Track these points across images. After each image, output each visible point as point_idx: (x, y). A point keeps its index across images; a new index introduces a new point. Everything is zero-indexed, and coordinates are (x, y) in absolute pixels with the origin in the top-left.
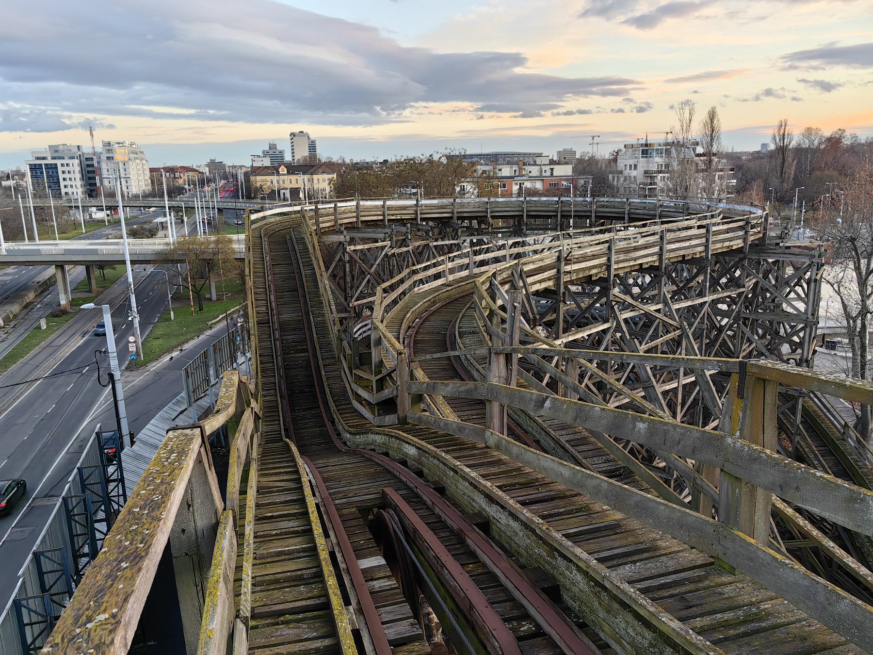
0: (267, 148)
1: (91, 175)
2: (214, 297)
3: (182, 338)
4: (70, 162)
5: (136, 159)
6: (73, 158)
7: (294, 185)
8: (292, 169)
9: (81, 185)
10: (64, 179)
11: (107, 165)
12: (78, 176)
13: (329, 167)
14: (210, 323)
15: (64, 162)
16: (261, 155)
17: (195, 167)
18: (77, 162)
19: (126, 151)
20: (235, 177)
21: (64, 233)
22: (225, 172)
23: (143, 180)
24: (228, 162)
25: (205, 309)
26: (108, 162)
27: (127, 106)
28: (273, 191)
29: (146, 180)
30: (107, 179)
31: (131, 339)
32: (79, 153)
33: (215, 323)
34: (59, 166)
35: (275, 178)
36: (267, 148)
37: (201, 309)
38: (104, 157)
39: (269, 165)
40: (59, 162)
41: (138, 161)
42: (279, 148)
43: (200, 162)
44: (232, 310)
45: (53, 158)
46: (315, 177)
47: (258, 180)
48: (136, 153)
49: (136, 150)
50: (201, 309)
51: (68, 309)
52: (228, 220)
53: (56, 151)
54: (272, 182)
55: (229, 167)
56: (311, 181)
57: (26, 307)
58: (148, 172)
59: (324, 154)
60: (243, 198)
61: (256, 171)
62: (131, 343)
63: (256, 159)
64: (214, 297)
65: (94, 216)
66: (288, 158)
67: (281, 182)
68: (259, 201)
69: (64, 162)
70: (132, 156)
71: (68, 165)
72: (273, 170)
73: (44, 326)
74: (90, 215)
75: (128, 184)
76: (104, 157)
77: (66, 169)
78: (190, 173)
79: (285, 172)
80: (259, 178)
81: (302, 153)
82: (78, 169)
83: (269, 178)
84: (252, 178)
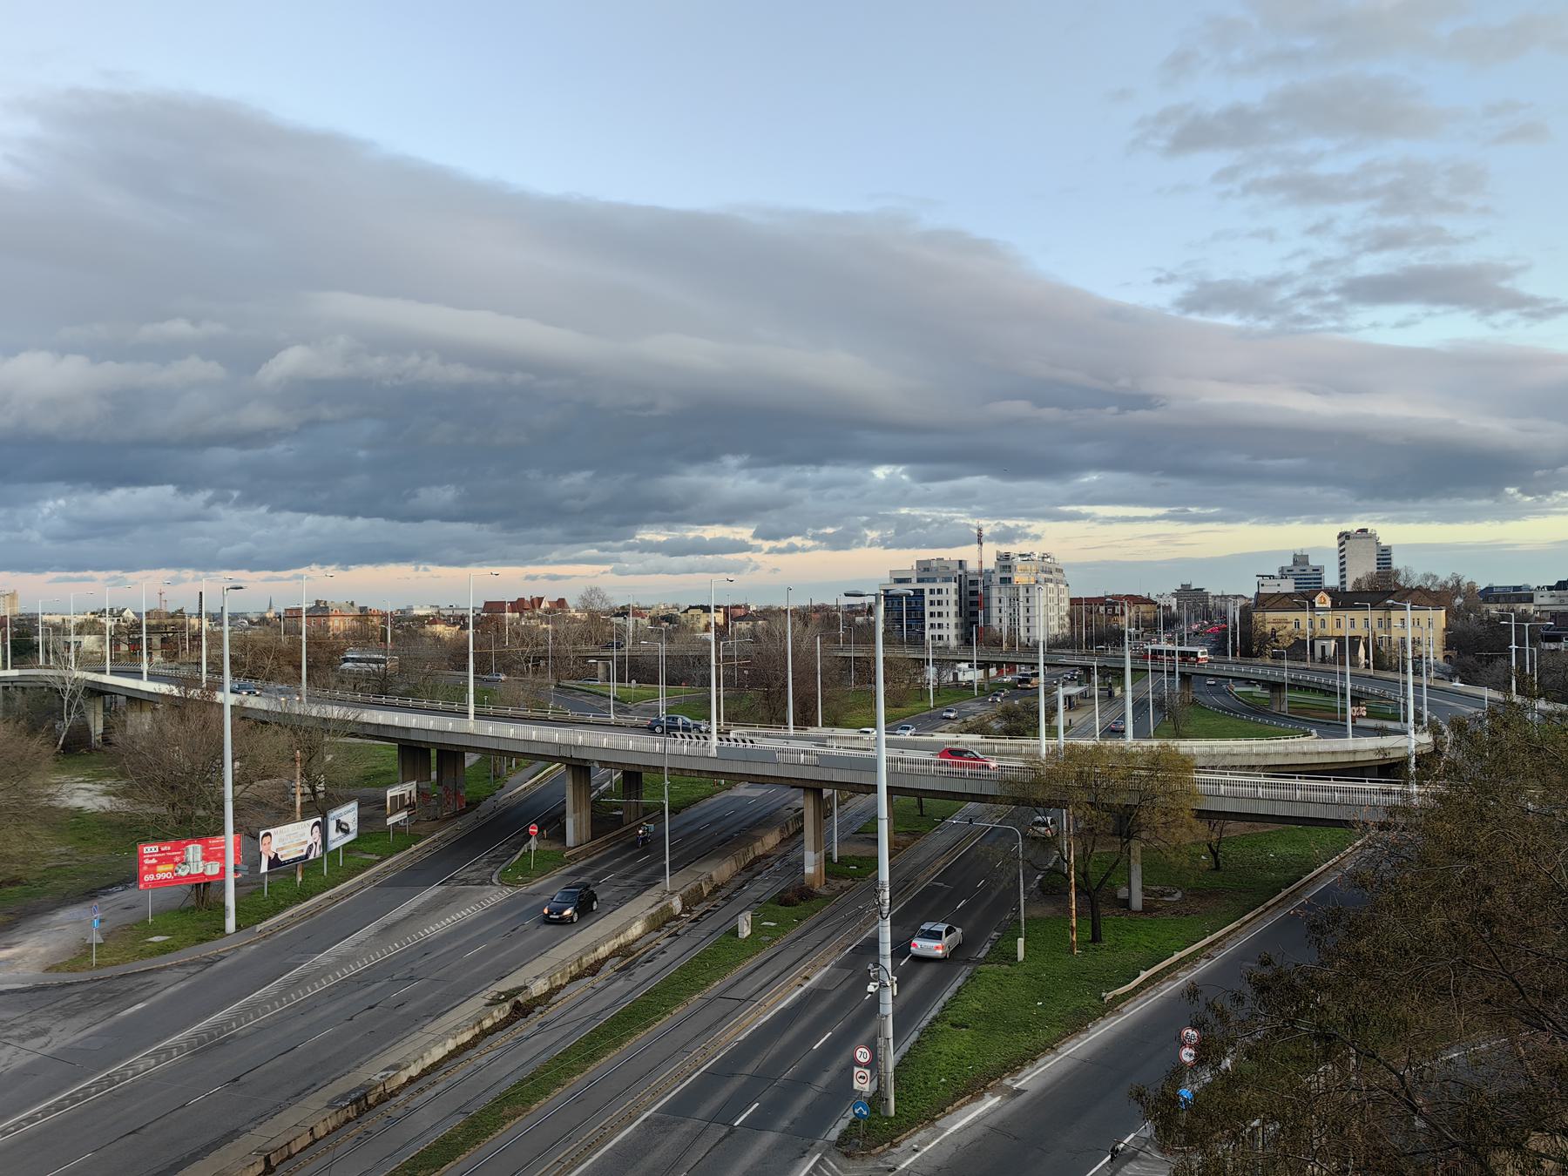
0: (1289, 563)
1: (973, 609)
2: (1137, 902)
3: (1025, 1041)
4: (943, 586)
5: (1047, 580)
6: (947, 580)
7: (1347, 632)
8: (1343, 600)
9: (956, 625)
10: (932, 614)
11: (1000, 592)
12: (953, 609)
13: (1425, 597)
14: (1110, 995)
15: (935, 586)
16: (1276, 574)
17: (1153, 597)
18: (954, 586)
19: (1033, 568)
20: (1223, 615)
21: (898, 707)
22: (1207, 606)
23: (1057, 618)
24: (1213, 589)
25: (1108, 938)
26: (1003, 585)
27: (1060, 508)
28: (1300, 643)
29: (1061, 618)
30: (998, 617)
31: (863, 1055)
32: (960, 572)
33: (1125, 997)
34: (927, 593)
35: (1304, 617)
36: (1289, 563)
37: (1096, 938)
38: (996, 579)
39: (1293, 590)
40: (927, 587)
41: (1051, 585)
42: (1313, 562)
43: (1163, 590)
44: (1177, 956)
45: (919, 581)
46: (1395, 616)
47: (1269, 620)
48: (1050, 571)
49: (1051, 566)
50: (1096, 938)
51: (818, 887)
52: (1201, 698)
53: (927, 570)
54: (1297, 625)
55: (1215, 597)
56: (1386, 624)
57: (749, 867)
58: (1066, 605)
59: (1412, 569)
60: (1234, 655)
61: (1264, 602)
62: (860, 1065)
63: (1267, 581)
64: (1137, 902)
65: (960, 678)
66: (1331, 579)
67: (1318, 624)
68: (1268, 661)
69: (935, 586)
70: (1042, 576)
71: (940, 591)
72: (1303, 599)
73: (745, 931)
74: (955, 675)
75: (1030, 624)
76: (996, 579)
77: (936, 597)
78: (1143, 608)
79: (1329, 604)
80: (1270, 616)
81: (1362, 568)
82: (954, 597)
83: (1291, 616)
84: (1257, 616)
